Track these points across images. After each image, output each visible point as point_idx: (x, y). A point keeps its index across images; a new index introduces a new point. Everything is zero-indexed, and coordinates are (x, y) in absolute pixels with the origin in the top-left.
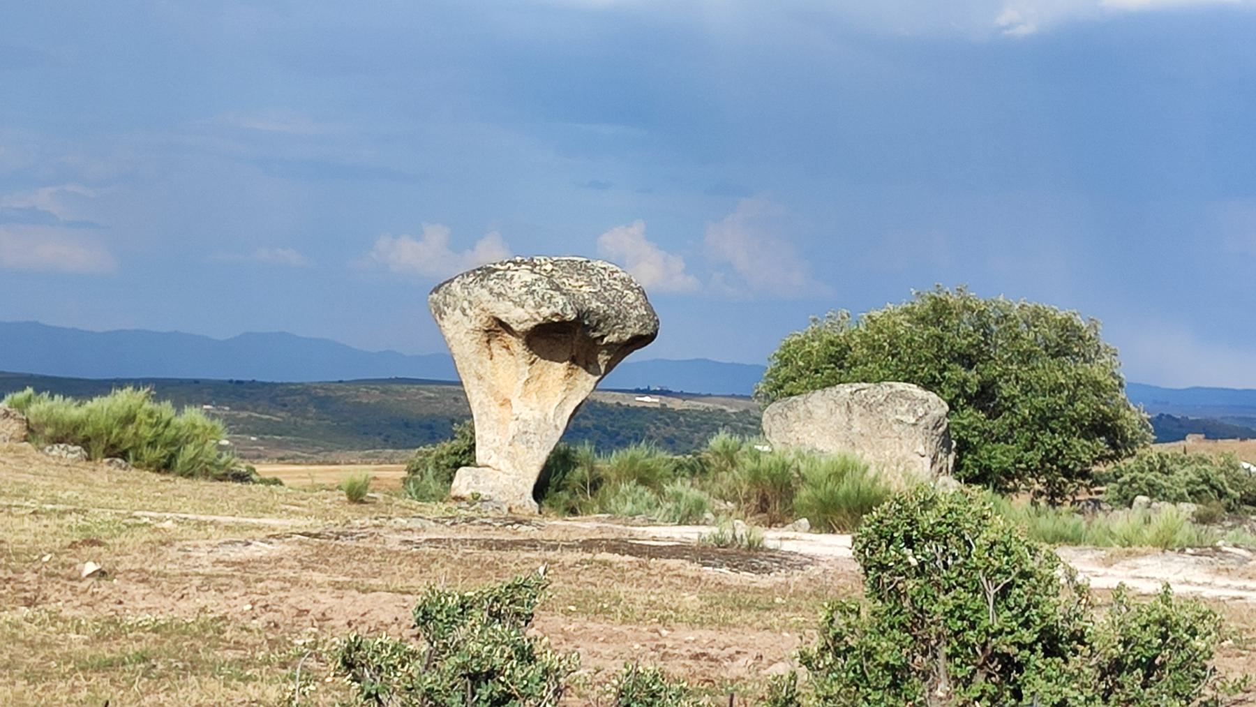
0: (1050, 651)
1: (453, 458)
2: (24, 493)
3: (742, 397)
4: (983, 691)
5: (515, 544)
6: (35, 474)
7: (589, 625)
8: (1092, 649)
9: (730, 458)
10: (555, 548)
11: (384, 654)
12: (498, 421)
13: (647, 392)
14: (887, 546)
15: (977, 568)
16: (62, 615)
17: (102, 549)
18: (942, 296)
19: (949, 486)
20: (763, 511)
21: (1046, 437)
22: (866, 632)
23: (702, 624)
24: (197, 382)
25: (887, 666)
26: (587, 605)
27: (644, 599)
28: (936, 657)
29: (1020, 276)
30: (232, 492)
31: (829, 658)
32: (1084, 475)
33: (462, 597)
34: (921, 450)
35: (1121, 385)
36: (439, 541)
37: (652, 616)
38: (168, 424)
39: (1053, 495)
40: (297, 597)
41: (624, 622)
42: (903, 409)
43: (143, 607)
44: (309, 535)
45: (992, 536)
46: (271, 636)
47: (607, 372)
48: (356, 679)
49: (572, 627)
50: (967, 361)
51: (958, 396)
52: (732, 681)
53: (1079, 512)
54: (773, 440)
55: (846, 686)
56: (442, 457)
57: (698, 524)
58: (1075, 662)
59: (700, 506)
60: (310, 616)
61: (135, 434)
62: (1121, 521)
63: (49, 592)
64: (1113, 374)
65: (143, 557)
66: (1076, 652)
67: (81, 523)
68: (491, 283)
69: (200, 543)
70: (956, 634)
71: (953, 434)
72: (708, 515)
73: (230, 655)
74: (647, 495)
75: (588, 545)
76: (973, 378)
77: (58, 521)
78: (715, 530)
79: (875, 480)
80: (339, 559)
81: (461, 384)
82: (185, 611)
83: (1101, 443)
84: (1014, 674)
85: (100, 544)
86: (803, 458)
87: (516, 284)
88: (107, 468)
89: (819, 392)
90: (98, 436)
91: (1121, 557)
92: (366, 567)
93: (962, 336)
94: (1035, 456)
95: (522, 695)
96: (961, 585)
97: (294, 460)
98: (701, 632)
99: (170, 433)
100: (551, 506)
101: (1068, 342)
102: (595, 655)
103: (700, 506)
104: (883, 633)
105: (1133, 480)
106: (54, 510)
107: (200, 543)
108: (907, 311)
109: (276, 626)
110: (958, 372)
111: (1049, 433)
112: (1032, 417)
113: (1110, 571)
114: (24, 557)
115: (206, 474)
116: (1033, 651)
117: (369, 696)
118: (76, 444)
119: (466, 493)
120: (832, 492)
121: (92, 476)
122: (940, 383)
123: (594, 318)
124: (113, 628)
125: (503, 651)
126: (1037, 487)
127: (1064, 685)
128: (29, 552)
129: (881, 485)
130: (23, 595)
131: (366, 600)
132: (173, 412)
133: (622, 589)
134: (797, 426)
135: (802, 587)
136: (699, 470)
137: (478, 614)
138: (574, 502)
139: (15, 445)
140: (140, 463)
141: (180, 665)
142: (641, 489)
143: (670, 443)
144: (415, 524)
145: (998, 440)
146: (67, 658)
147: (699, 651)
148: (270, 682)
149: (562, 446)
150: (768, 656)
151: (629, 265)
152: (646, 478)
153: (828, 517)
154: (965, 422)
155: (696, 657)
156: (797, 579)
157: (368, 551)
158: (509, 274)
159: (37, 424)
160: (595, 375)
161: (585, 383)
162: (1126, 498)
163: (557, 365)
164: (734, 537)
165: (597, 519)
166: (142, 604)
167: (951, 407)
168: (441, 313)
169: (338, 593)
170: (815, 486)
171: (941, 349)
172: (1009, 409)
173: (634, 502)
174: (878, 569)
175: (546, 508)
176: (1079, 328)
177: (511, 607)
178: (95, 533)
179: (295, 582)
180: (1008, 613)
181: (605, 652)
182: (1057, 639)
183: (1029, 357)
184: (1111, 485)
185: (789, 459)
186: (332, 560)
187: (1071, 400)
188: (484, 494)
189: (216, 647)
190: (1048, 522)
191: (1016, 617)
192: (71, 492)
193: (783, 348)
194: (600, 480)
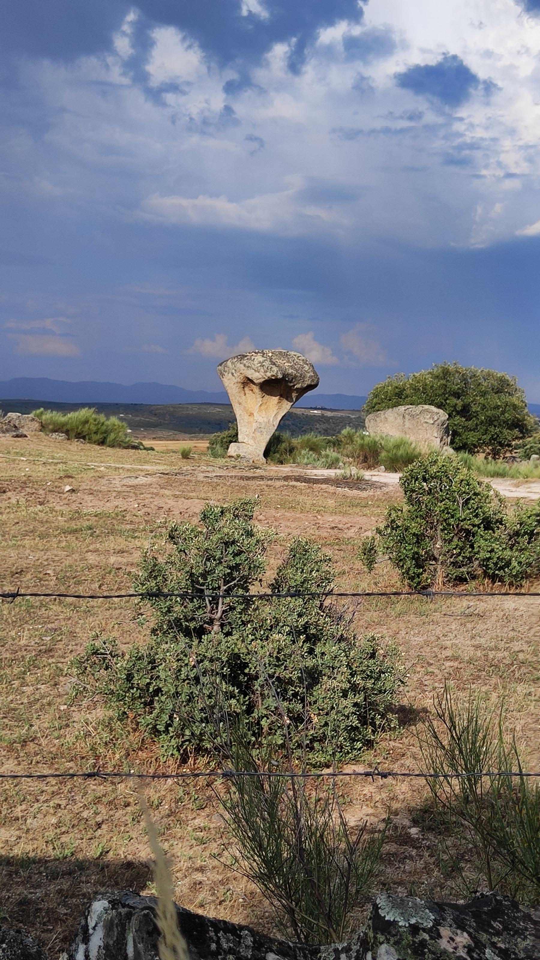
0: (486, 528)
1: (229, 439)
2: (40, 455)
3: (357, 411)
4: (457, 545)
5: (254, 478)
6: (45, 446)
7: (286, 514)
8: (505, 526)
9: (350, 438)
10: (271, 479)
11: (187, 533)
12: (248, 423)
13: (316, 409)
14: (415, 482)
15: (455, 491)
16: (55, 509)
17: (73, 480)
18: (446, 367)
19: (449, 451)
20: (366, 462)
21: (492, 429)
22: (405, 520)
23: (336, 513)
24: (117, 404)
25: (414, 534)
26: (285, 505)
27: (310, 502)
28: (436, 530)
29: (482, 357)
30: (131, 454)
31: (389, 531)
32: (509, 445)
33: (222, 508)
34: (436, 435)
35: (526, 405)
36: (221, 476)
37: (314, 510)
38: (103, 424)
39: (495, 455)
40: (158, 501)
41: (301, 512)
42: (428, 417)
43: (91, 505)
44: (164, 474)
45: (462, 477)
46: (146, 519)
47: (296, 401)
48: (175, 543)
49: (279, 515)
50: (457, 395)
51: (453, 411)
52: (348, 539)
53: (507, 462)
54: (370, 431)
55: (396, 543)
56: (224, 438)
57: (336, 468)
58: (498, 533)
59: (337, 460)
60: (163, 510)
61: (89, 429)
62: (524, 466)
63: (50, 499)
64: (522, 401)
65: (91, 483)
66: (498, 528)
67: (64, 468)
68: (245, 362)
69: (116, 477)
70: (445, 520)
71: (451, 428)
72: (341, 464)
73: (128, 527)
74: (314, 455)
75: (286, 478)
76: (459, 403)
77: (54, 467)
78: (343, 471)
79: (414, 449)
80: (176, 484)
81: (231, 405)
82: (108, 507)
83: (516, 432)
84: (471, 538)
85: (72, 477)
86: (383, 439)
87: (256, 362)
88: (76, 443)
89: (391, 409)
90: (72, 429)
91: (523, 483)
92: (188, 488)
93: (456, 384)
94: (487, 437)
95: (247, 551)
96: (448, 499)
97: (160, 439)
98: (335, 517)
99: (104, 428)
100: (272, 460)
101: (502, 387)
102: (288, 527)
103: (337, 460)
104: (413, 520)
105: (531, 447)
106: (52, 462)
107: (116, 477)
108: (430, 373)
109: (149, 514)
110: (453, 401)
111: (493, 427)
112: (483, 421)
113: (518, 489)
114: (39, 483)
115: (120, 446)
116: (479, 528)
117: (181, 551)
118: (63, 433)
119: (234, 454)
120: (395, 454)
121: (70, 447)
122: (444, 405)
123: (290, 377)
124: (77, 515)
125: (239, 532)
126: (488, 451)
127: (493, 543)
128: (41, 481)
129: (418, 450)
130: (38, 500)
131: (188, 503)
132: (105, 419)
133: (300, 498)
134: (381, 425)
135: (380, 497)
136: (337, 444)
137: (228, 515)
138: (282, 458)
139: (37, 433)
140: (91, 441)
141: (107, 531)
142: (311, 452)
143: (326, 432)
144: (210, 469)
145: (471, 430)
146: (57, 528)
147: (334, 525)
148: (145, 539)
149: (277, 433)
150: (364, 528)
151: (307, 353)
152: (314, 448)
153: (393, 465)
154: (456, 423)
155: (333, 528)
156: (378, 493)
157: (189, 481)
158: (253, 357)
159: (46, 424)
160: (291, 402)
161: (286, 406)
162: (528, 455)
163: (274, 398)
164: (351, 475)
165: (291, 466)
166: (91, 504)
167: (450, 415)
168: (223, 375)
169: (176, 499)
170: (388, 451)
171: (445, 390)
172: (475, 417)
173: (308, 458)
174: (411, 492)
175: (269, 461)
176: (508, 381)
177: (244, 512)
178: (70, 473)
179: (157, 494)
180: (468, 511)
181: (293, 526)
182: (489, 522)
183: (485, 393)
184: (522, 450)
185: (377, 439)
186: (173, 485)
187: (503, 413)
188: (242, 455)
189: (122, 523)
190: (491, 467)
191: (472, 513)
192: (60, 454)
193: (375, 390)
194: (293, 449)
